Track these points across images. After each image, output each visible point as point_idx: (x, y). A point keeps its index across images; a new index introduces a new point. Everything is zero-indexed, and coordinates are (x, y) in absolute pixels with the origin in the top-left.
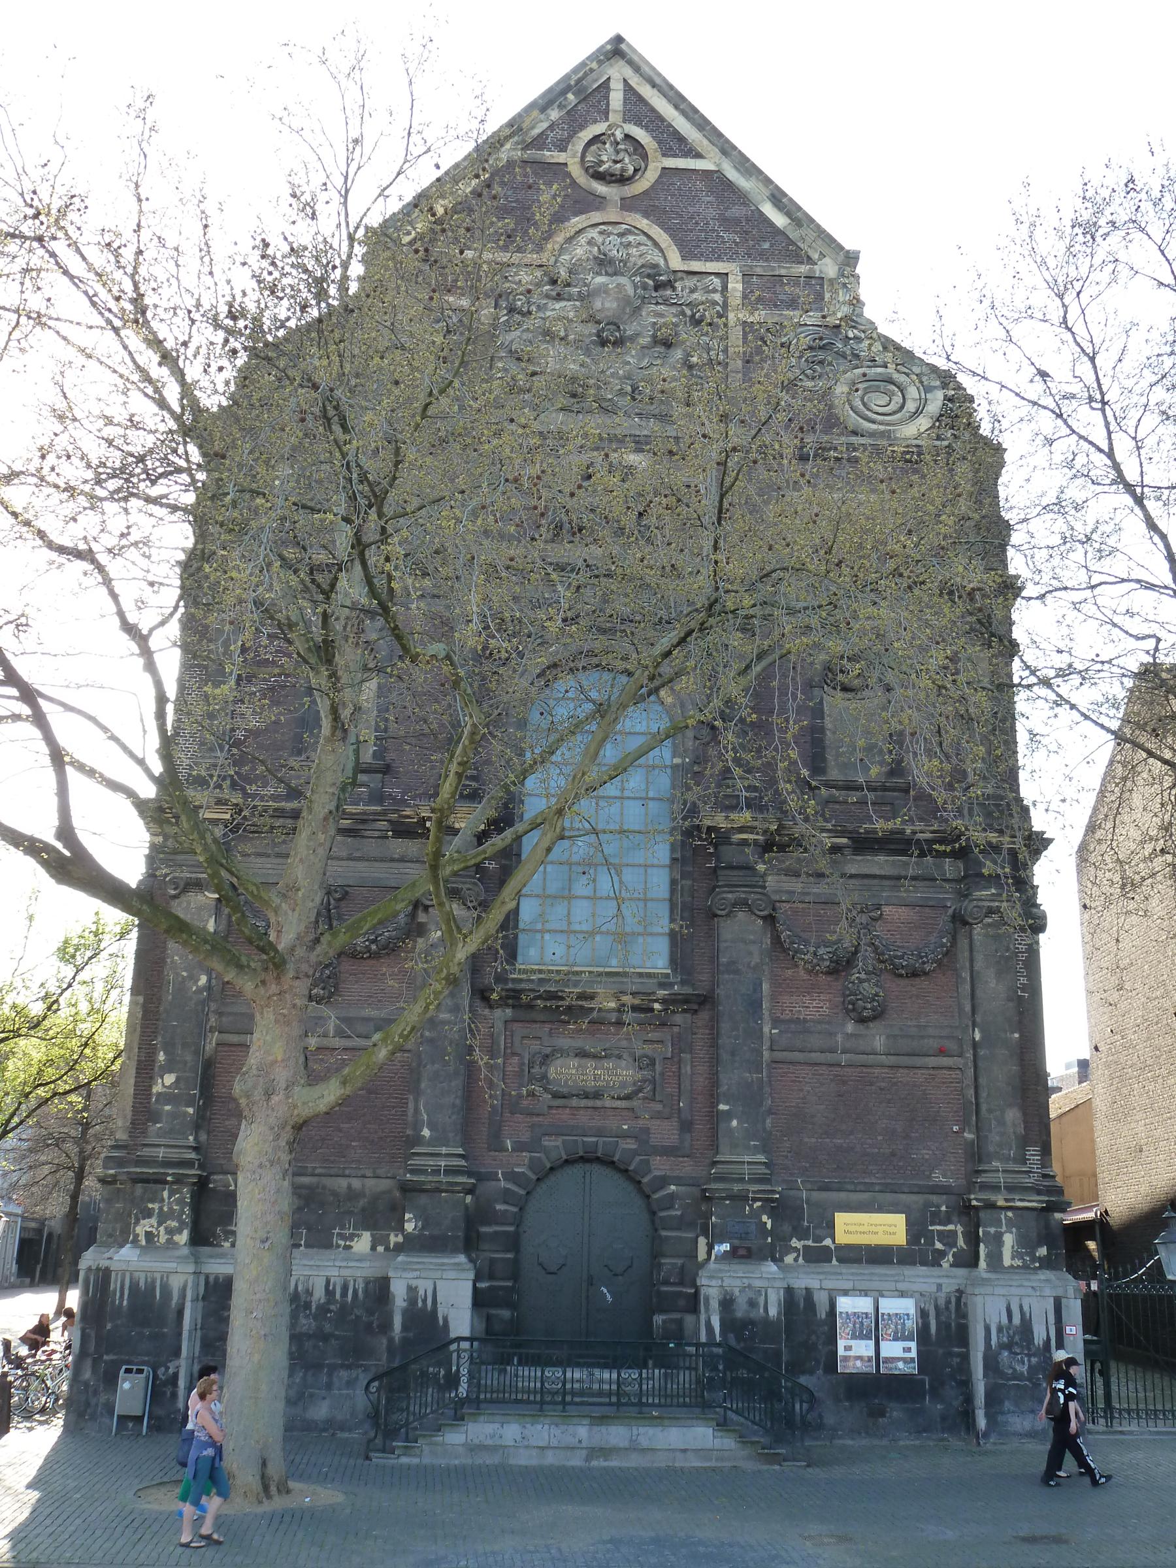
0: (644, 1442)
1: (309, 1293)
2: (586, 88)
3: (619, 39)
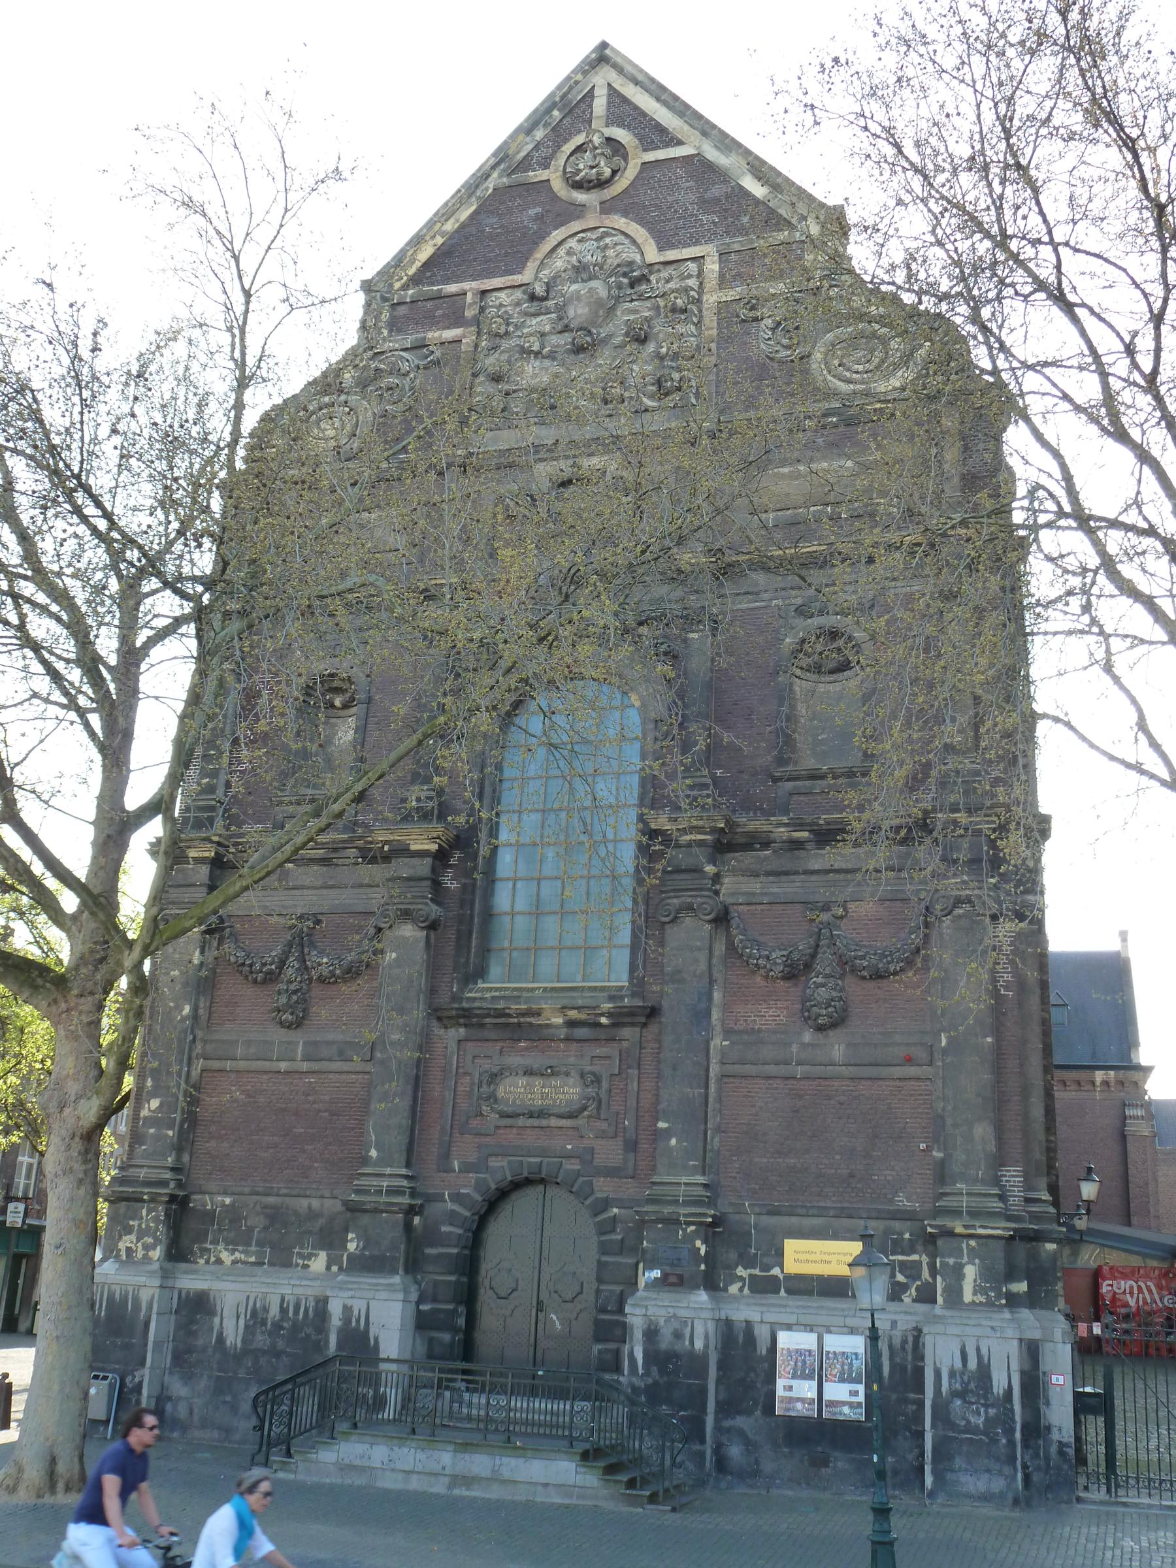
0: (506, 1474)
1: (266, 1309)
2: (570, 101)
3: (604, 45)
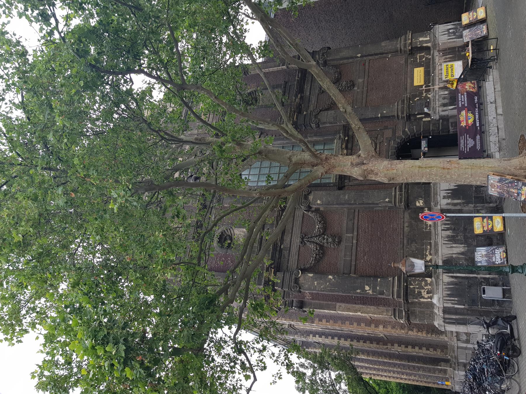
1: (448, 237)
